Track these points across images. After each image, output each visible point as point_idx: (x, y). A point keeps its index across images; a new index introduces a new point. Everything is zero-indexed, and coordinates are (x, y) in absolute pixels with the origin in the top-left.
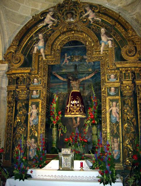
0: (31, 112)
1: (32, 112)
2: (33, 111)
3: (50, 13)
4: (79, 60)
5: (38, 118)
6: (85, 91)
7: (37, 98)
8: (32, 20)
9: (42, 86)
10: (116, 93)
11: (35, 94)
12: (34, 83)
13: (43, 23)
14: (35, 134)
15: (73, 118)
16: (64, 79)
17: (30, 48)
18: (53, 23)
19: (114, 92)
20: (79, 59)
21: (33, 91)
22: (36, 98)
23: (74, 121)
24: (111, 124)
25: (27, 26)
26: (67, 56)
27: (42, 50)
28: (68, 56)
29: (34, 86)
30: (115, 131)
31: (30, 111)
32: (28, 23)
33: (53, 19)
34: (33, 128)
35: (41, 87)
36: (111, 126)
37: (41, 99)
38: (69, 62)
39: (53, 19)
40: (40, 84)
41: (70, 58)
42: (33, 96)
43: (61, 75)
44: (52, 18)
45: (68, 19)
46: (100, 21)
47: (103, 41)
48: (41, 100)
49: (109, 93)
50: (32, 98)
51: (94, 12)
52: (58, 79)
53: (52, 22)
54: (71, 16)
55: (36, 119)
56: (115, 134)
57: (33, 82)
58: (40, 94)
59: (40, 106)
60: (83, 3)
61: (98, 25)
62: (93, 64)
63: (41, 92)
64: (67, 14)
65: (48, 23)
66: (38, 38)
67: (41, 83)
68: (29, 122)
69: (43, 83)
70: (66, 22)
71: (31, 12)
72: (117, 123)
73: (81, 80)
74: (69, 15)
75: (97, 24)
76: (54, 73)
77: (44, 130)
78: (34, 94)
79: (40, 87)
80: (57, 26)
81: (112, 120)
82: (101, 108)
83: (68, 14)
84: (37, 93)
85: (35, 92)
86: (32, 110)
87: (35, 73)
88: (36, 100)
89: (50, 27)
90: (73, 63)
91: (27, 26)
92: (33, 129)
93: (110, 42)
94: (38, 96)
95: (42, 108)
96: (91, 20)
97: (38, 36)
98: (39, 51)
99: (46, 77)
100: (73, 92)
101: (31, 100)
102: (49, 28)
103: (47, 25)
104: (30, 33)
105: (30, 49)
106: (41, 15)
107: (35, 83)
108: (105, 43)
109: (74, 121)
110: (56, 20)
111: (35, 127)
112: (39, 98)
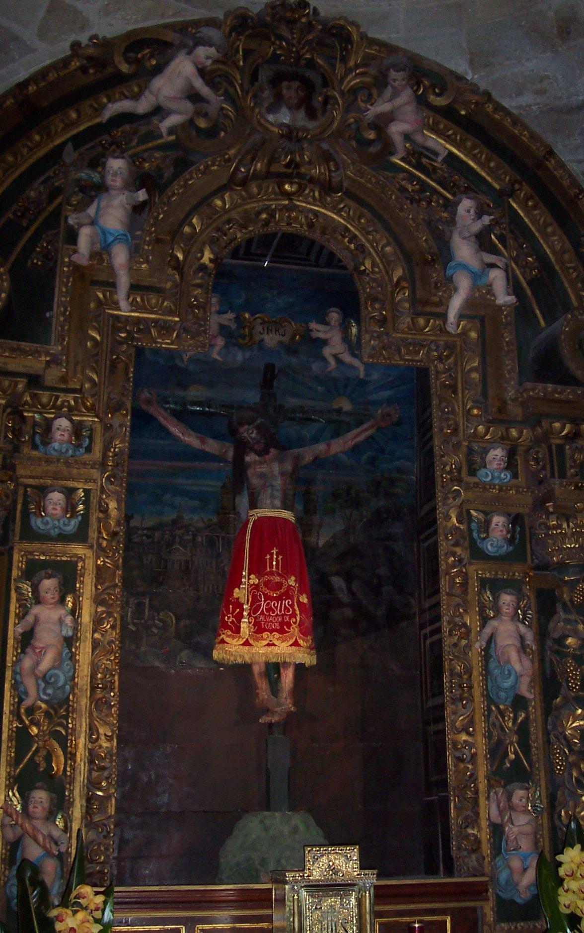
0: (30, 618)
1: (37, 620)
2: (42, 618)
3: (202, 52)
4: (280, 343)
5: (72, 657)
6: (316, 519)
7: (65, 538)
8: (66, 62)
9: (103, 465)
10: (511, 548)
11: (59, 512)
12: (46, 442)
13: (136, 97)
14: (49, 758)
15: (256, 669)
16: (203, 441)
17: (27, 228)
18: (198, 113)
19: (505, 539)
20: (286, 339)
21: (43, 490)
22: (60, 535)
23: (263, 687)
24: (490, 711)
25: (32, 89)
26: (220, 312)
27: (120, 256)
28: (226, 312)
29: (49, 461)
30: (511, 749)
31: (21, 617)
32: (42, 74)
33: (205, 91)
34: (38, 725)
35: (95, 473)
36: (492, 719)
37: (91, 547)
38: (226, 346)
39: (205, 91)
40: (86, 456)
41: (233, 326)
42: (37, 523)
43: (182, 416)
44: (199, 84)
45: (284, 110)
46: (440, 159)
47: (465, 267)
48: (89, 553)
49: (480, 546)
50: (29, 534)
51: (421, 101)
52: (169, 433)
53: (188, 106)
54: (301, 94)
55: (59, 667)
56: (511, 762)
57: (38, 439)
58: (86, 516)
59: (87, 586)
60: (373, 42)
61: (428, 175)
62: (362, 375)
63: (94, 501)
64: (276, 81)
65: (167, 105)
66: (103, 177)
67: (89, 449)
68: (7, 686)
69: (106, 448)
70: (270, 126)
71: (41, 13)
72: (519, 703)
73: (308, 454)
74: (290, 91)
75: (419, 167)
76: (149, 402)
77: (109, 739)
78: (50, 508)
79: (82, 471)
80: (211, 133)
81: (499, 688)
82: (124, 579)
83: (285, 84)
84: (70, 507)
85: (56, 497)
86: (36, 610)
87: (64, 379)
88: (59, 547)
89: (171, 131)
90: (248, 355)
91: (32, 89)
92: (34, 730)
93: (497, 278)
94: (72, 526)
95: (98, 600)
96: (398, 140)
97: (104, 165)
98: (101, 254)
99: (126, 415)
100: (261, 519)
101: (28, 546)
102: (164, 131)
103: (159, 111)
104: (37, 138)
105: (29, 234)
106: (128, 49)
107: (56, 445)
108: (475, 277)
109: (263, 687)
110: (214, 100)
111: (47, 714)
112: (80, 536)
